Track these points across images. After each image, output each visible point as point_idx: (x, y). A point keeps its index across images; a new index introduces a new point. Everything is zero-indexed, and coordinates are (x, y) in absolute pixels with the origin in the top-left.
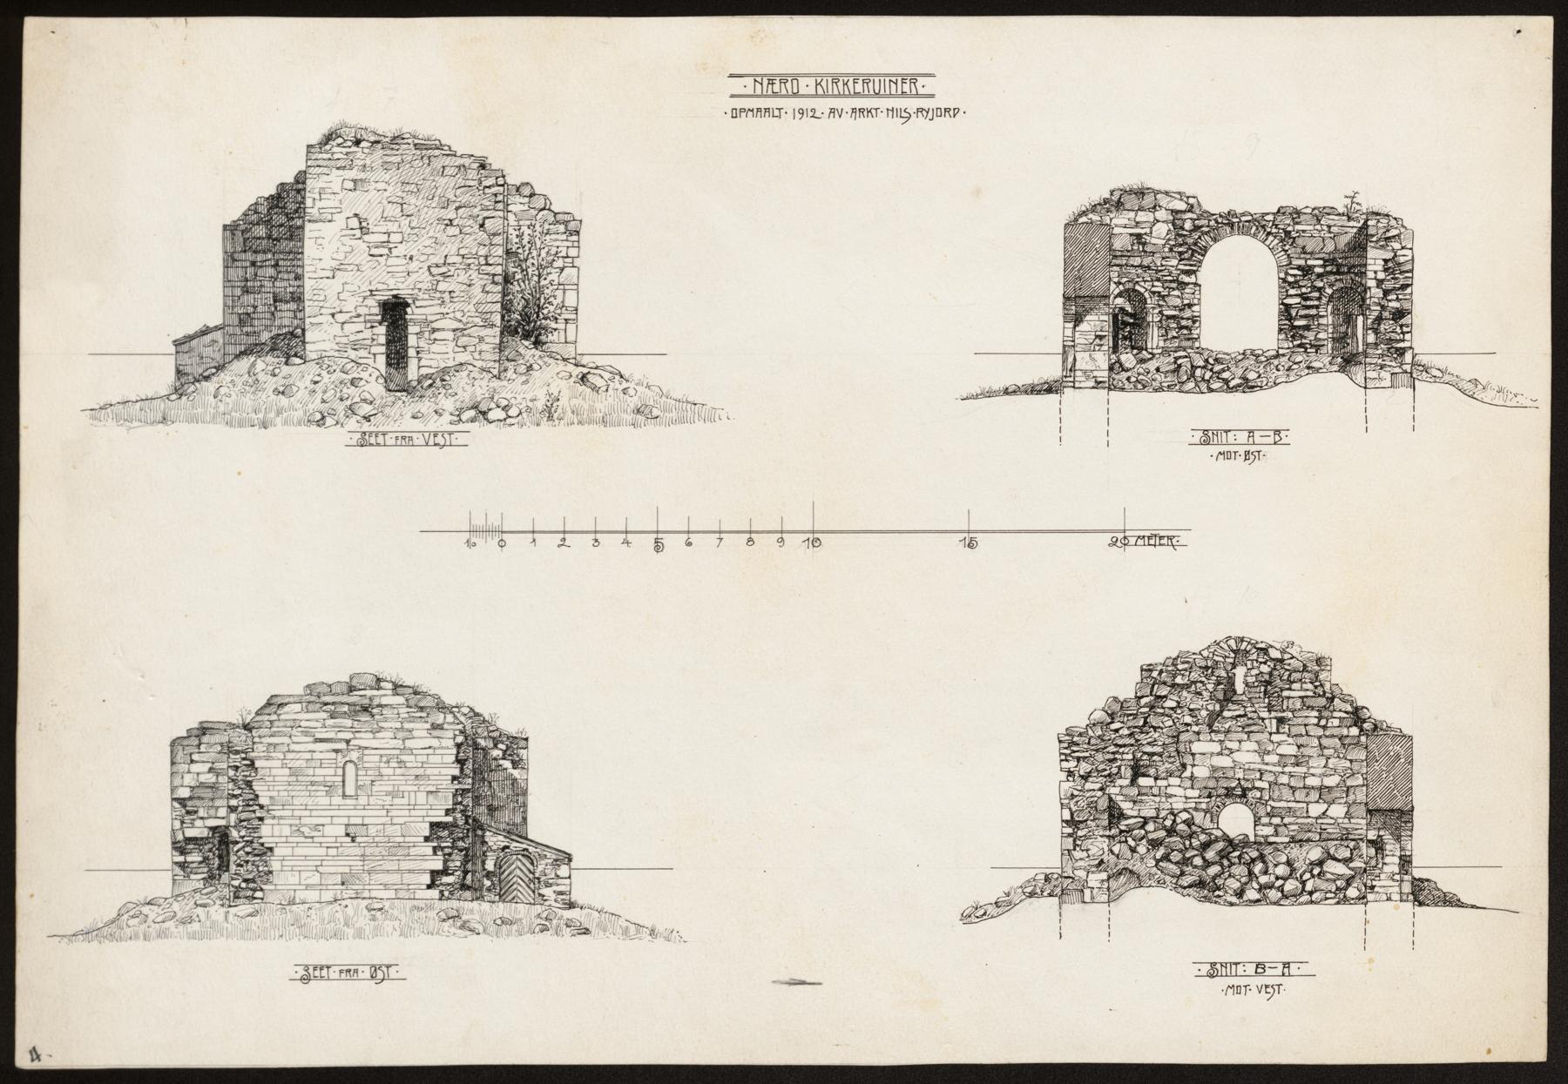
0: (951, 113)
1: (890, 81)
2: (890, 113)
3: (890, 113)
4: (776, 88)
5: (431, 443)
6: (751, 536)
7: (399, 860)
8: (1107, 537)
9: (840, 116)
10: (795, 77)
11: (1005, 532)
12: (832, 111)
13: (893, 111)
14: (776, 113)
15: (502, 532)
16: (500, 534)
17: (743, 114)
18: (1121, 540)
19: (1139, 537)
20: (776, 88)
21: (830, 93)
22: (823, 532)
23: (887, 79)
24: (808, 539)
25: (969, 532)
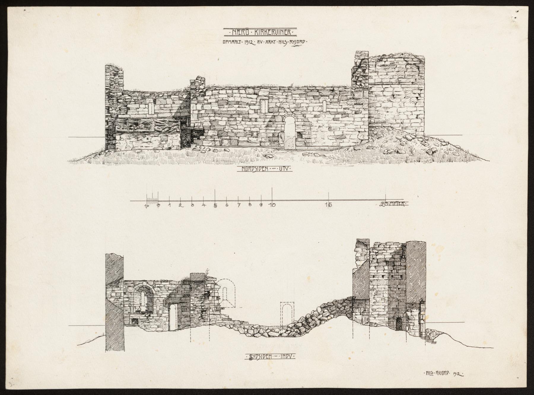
1: (281, 30)
3: (280, 42)
6: (250, 202)
8: (379, 203)
9: (261, 43)
10: (247, 29)
11: (311, 200)
12: (258, 41)
15: (158, 201)
16: (158, 203)
17: (227, 42)
18: (384, 203)
19: (391, 202)
21: (260, 35)
25: (329, 200)
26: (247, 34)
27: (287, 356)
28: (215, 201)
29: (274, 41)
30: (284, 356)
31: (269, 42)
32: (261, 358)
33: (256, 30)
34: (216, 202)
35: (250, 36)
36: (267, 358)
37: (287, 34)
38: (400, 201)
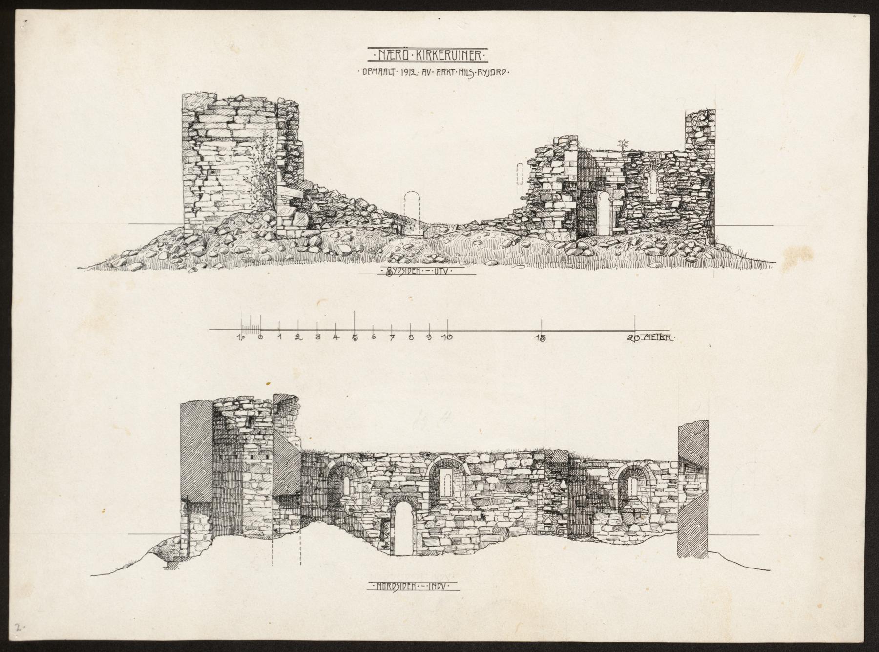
0: (501, 72)
1: (463, 52)
2: (461, 72)
4: (393, 56)
5: (411, 273)
7: (487, 527)
9: (429, 75)
10: (406, 49)
11: (467, 331)
12: (424, 71)
13: (463, 71)
14: (391, 72)
15: (261, 330)
16: (259, 331)
17: (370, 72)
19: (647, 335)
20: (393, 56)
22: (396, 330)
23: (461, 51)
24: (538, 336)
26: (405, 57)
27: (438, 586)
28: (373, 330)
29: (452, 70)
30: (434, 586)
31: (440, 71)
32: (399, 589)
33: (419, 51)
34: (412, 333)
35: (376, 48)
36: (409, 589)
37: (474, 59)
38: (663, 333)
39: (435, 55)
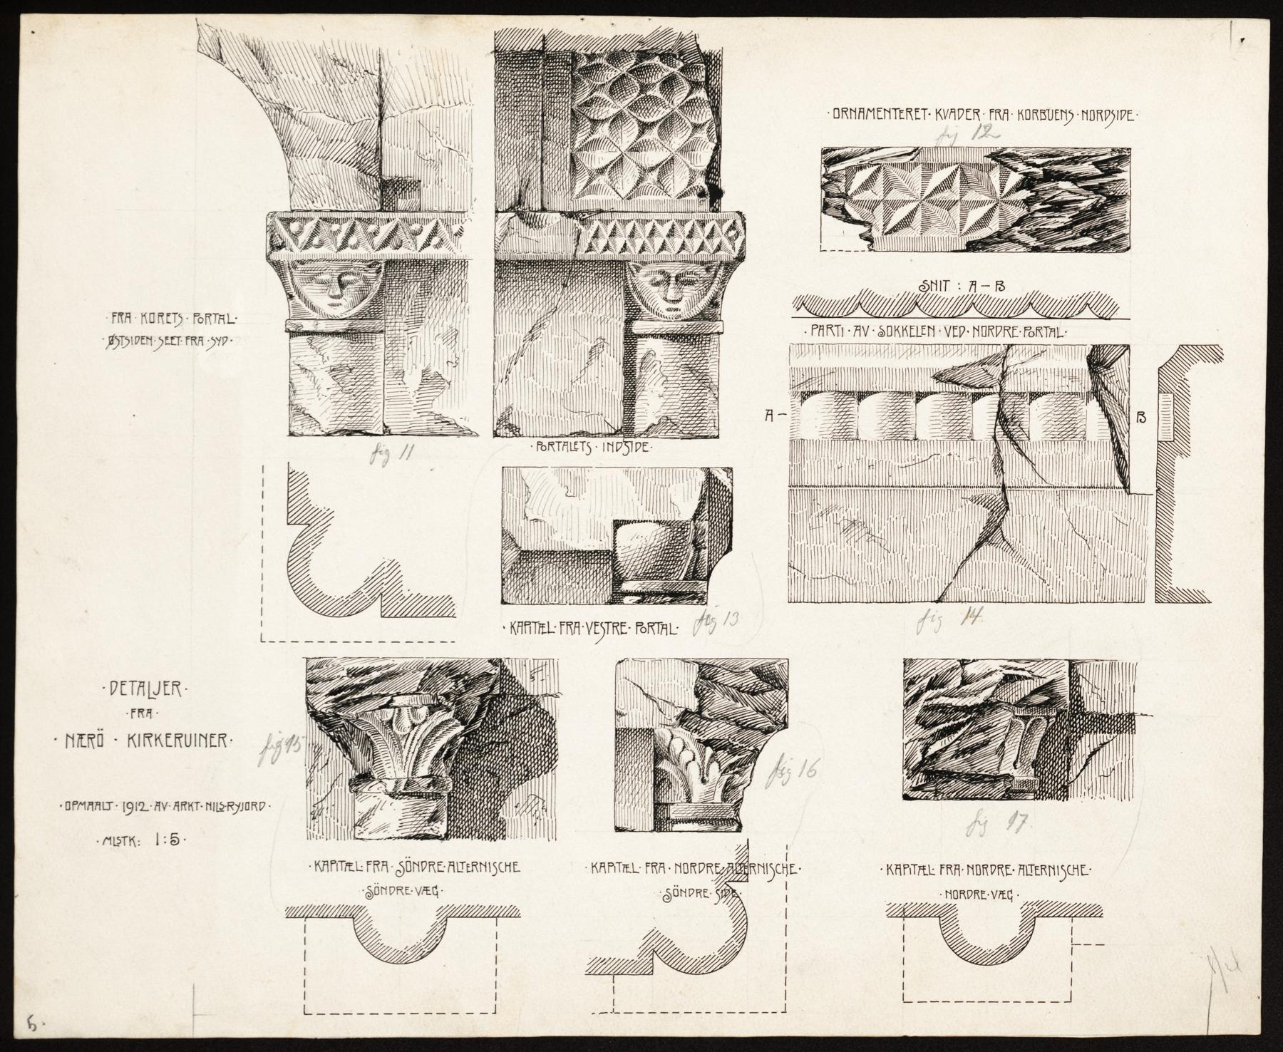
17: (76, 806)
39: (594, 868)
